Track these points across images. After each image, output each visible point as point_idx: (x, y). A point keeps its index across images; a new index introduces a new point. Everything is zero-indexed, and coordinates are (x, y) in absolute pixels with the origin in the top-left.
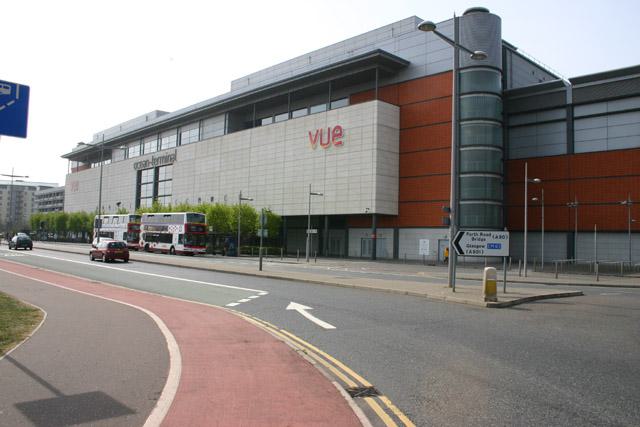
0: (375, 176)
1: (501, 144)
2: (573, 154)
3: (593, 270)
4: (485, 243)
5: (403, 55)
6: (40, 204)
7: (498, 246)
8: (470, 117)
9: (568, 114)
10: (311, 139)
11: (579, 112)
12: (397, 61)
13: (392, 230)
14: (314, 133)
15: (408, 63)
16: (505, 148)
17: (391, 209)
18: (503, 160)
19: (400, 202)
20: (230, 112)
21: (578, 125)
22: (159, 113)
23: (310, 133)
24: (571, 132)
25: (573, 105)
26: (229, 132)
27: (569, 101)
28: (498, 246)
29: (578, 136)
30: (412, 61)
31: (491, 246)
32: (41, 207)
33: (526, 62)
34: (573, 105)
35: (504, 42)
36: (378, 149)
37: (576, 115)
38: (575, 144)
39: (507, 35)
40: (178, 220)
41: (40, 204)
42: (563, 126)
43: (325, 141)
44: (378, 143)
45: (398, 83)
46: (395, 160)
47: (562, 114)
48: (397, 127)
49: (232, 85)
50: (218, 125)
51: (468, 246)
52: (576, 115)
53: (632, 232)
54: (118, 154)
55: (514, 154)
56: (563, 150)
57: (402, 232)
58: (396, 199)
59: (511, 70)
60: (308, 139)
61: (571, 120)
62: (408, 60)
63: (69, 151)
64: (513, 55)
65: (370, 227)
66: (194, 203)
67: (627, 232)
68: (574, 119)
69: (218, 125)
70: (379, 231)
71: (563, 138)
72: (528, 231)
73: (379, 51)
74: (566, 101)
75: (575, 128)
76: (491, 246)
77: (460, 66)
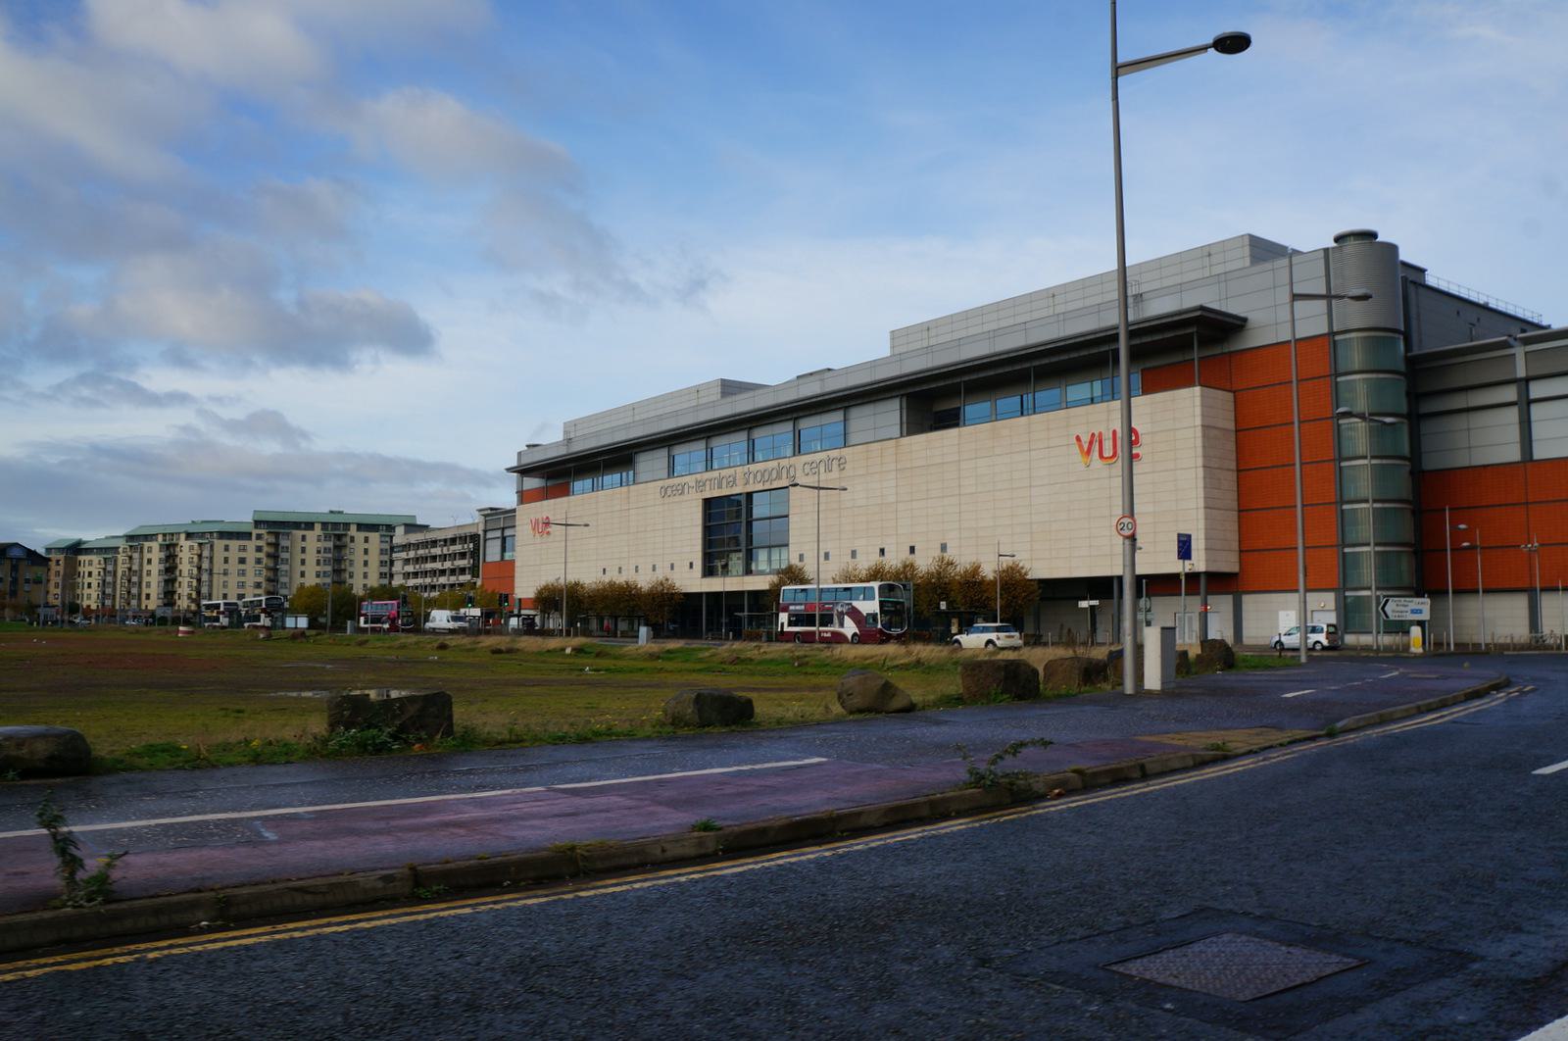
0: (1202, 511)
1: (1406, 450)
2: (1531, 460)
3: (709, 548)
4: (1408, 609)
5: (1234, 308)
6: (407, 561)
7: (1420, 612)
8: (1361, 369)
9: (1519, 394)
10: (1081, 447)
11: (1537, 390)
12: (1219, 317)
13: (1229, 599)
14: (1085, 439)
15: (1245, 320)
16: (1415, 455)
17: (1229, 564)
18: (1412, 473)
19: (1241, 551)
20: (908, 396)
21: (1536, 411)
22: (729, 388)
23: (1078, 439)
24: (1526, 424)
25: (1527, 380)
26: (909, 433)
27: (1521, 373)
28: (1420, 612)
29: (1537, 431)
30: (1250, 316)
31: (1414, 612)
32: (410, 568)
33: (1446, 298)
34: (1527, 380)
35: (1405, 264)
36: (1204, 467)
37: (1533, 395)
38: (1534, 445)
39: (1404, 256)
40: (867, 594)
41: (407, 561)
42: (1512, 415)
43: (1108, 452)
44: (1204, 456)
45: (1230, 353)
46: (1229, 480)
47: (1510, 394)
48: (1231, 426)
49: (893, 339)
50: (890, 413)
51: (1393, 611)
52: (1533, 395)
53: (1053, 644)
54: (650, 464)
55: (1431, 463)
56: (1512, 454)
57: (1248, 601)
58: (1235, 545)
59: (1418, 315)
60: (1076, 449)
61: (1525, 404)
62: (1242, 315)
63: (514, 463)
64: (1422, 291)
65: (1198, 594)
66: (894, 560)
67: (1477, 592)
68: (1530, 402)
69: (890, 413)
70: (1210, 598)
71: (1513, 433)
72: (1453, 592)
73: (1202, 308)
74: (1515, 372)
75: (1533, 417)
76: (1414, 612)
77: (1335, 330)
